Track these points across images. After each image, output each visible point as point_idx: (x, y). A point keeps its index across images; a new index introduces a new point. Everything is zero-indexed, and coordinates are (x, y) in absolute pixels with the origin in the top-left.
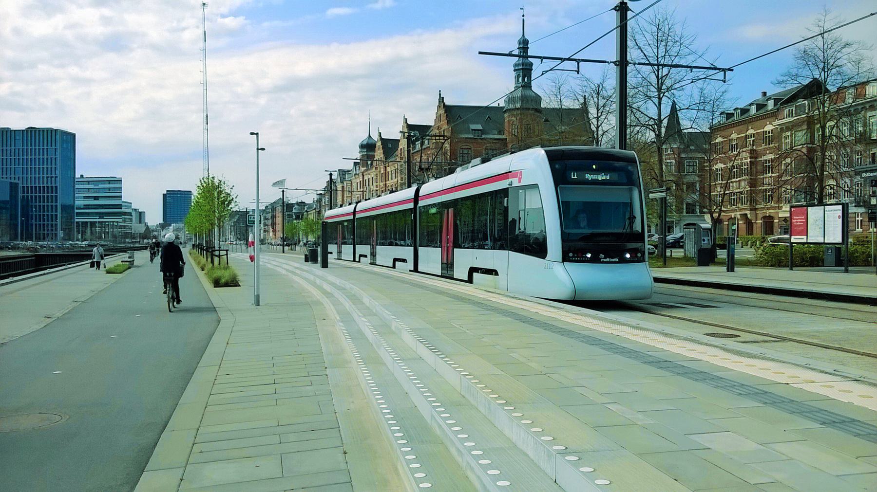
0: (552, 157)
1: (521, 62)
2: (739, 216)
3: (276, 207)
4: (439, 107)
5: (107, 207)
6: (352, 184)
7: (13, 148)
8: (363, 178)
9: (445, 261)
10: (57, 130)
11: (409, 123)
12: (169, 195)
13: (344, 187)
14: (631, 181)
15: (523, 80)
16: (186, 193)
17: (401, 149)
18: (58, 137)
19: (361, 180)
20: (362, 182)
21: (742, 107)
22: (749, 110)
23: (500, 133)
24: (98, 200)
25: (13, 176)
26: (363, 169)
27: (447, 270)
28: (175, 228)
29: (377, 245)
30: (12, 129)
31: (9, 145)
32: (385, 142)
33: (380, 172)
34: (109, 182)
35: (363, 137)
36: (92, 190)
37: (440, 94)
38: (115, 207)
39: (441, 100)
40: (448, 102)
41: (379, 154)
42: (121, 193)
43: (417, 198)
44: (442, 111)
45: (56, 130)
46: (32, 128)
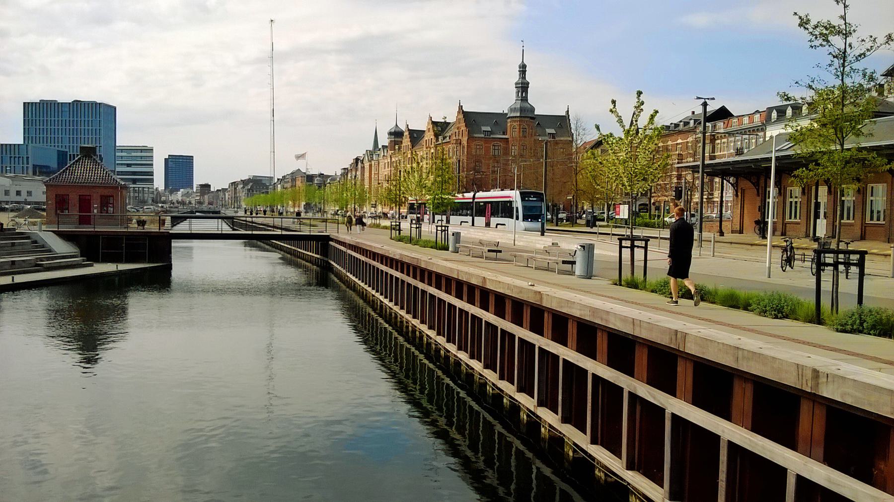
0: (521, 193)
1: (521, 81)
2: (669, 200)
3: (296, 178)
4: (459, 112)
5: (143, 174)
6: (379, 163)
7: (60, 119)
8: (391, 160)
9: (487, 222)
10: (101, 103)
11: (433, 120)
12: (171, 160)
13: (372, 165)
14: (542, 200)
15: (522, 94)
16: (177, 157)
17: (426, 140)
18: (102, 110)
19: (389, 161)
20: (390, 163)
21: (676, 122)
22: (688, 123)
23: (504, 133)
24: (131, 167)
25: (60, 144)
26: (390, 152)
27: (488, 224)
28: (183, 194)
29: (450, 215)
30: (58, 102)
31: (56, 116)
32: (412, 132)
33: (407, 156)
34: (141, 151)
35: (391, 127)
36: (125, 157)
37: (460, 103)
38: (147, 174)
39: (461, 107)
40: (465, 109)
41: (406, 141)
42: (153, 161)
43: (474, 198)
44: (461, 116)
45: (100, 104)
46: (77, 101)
